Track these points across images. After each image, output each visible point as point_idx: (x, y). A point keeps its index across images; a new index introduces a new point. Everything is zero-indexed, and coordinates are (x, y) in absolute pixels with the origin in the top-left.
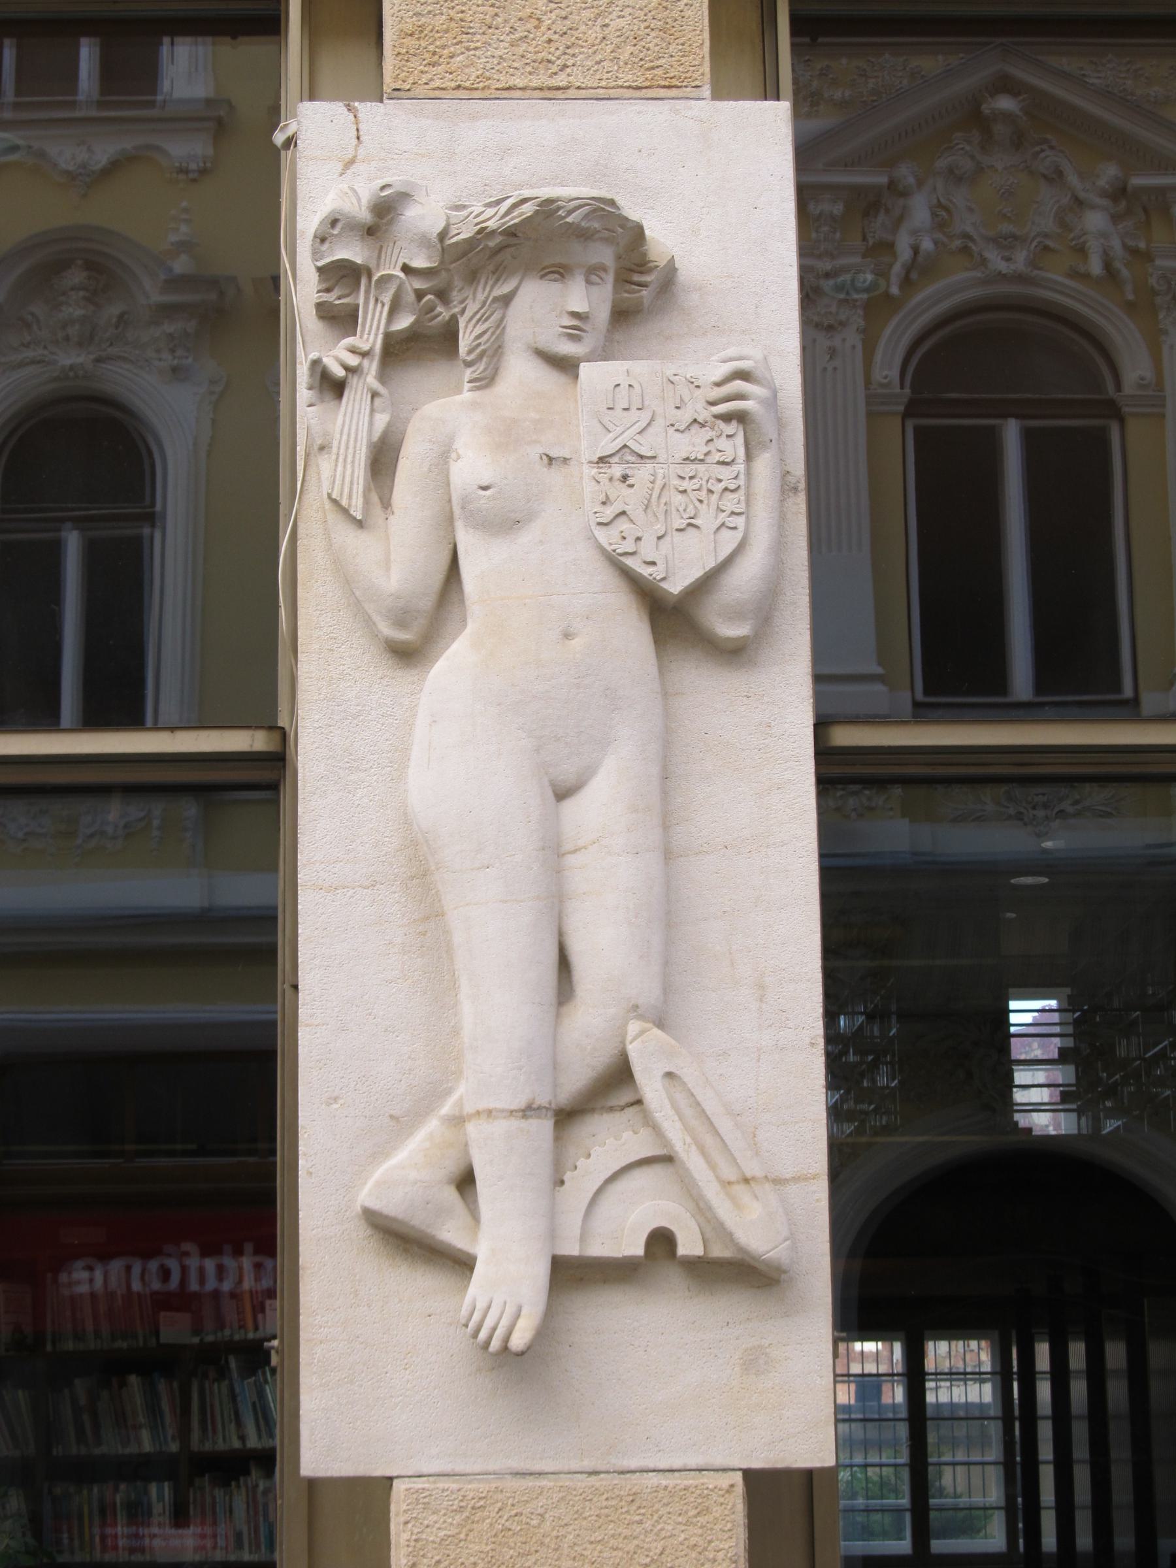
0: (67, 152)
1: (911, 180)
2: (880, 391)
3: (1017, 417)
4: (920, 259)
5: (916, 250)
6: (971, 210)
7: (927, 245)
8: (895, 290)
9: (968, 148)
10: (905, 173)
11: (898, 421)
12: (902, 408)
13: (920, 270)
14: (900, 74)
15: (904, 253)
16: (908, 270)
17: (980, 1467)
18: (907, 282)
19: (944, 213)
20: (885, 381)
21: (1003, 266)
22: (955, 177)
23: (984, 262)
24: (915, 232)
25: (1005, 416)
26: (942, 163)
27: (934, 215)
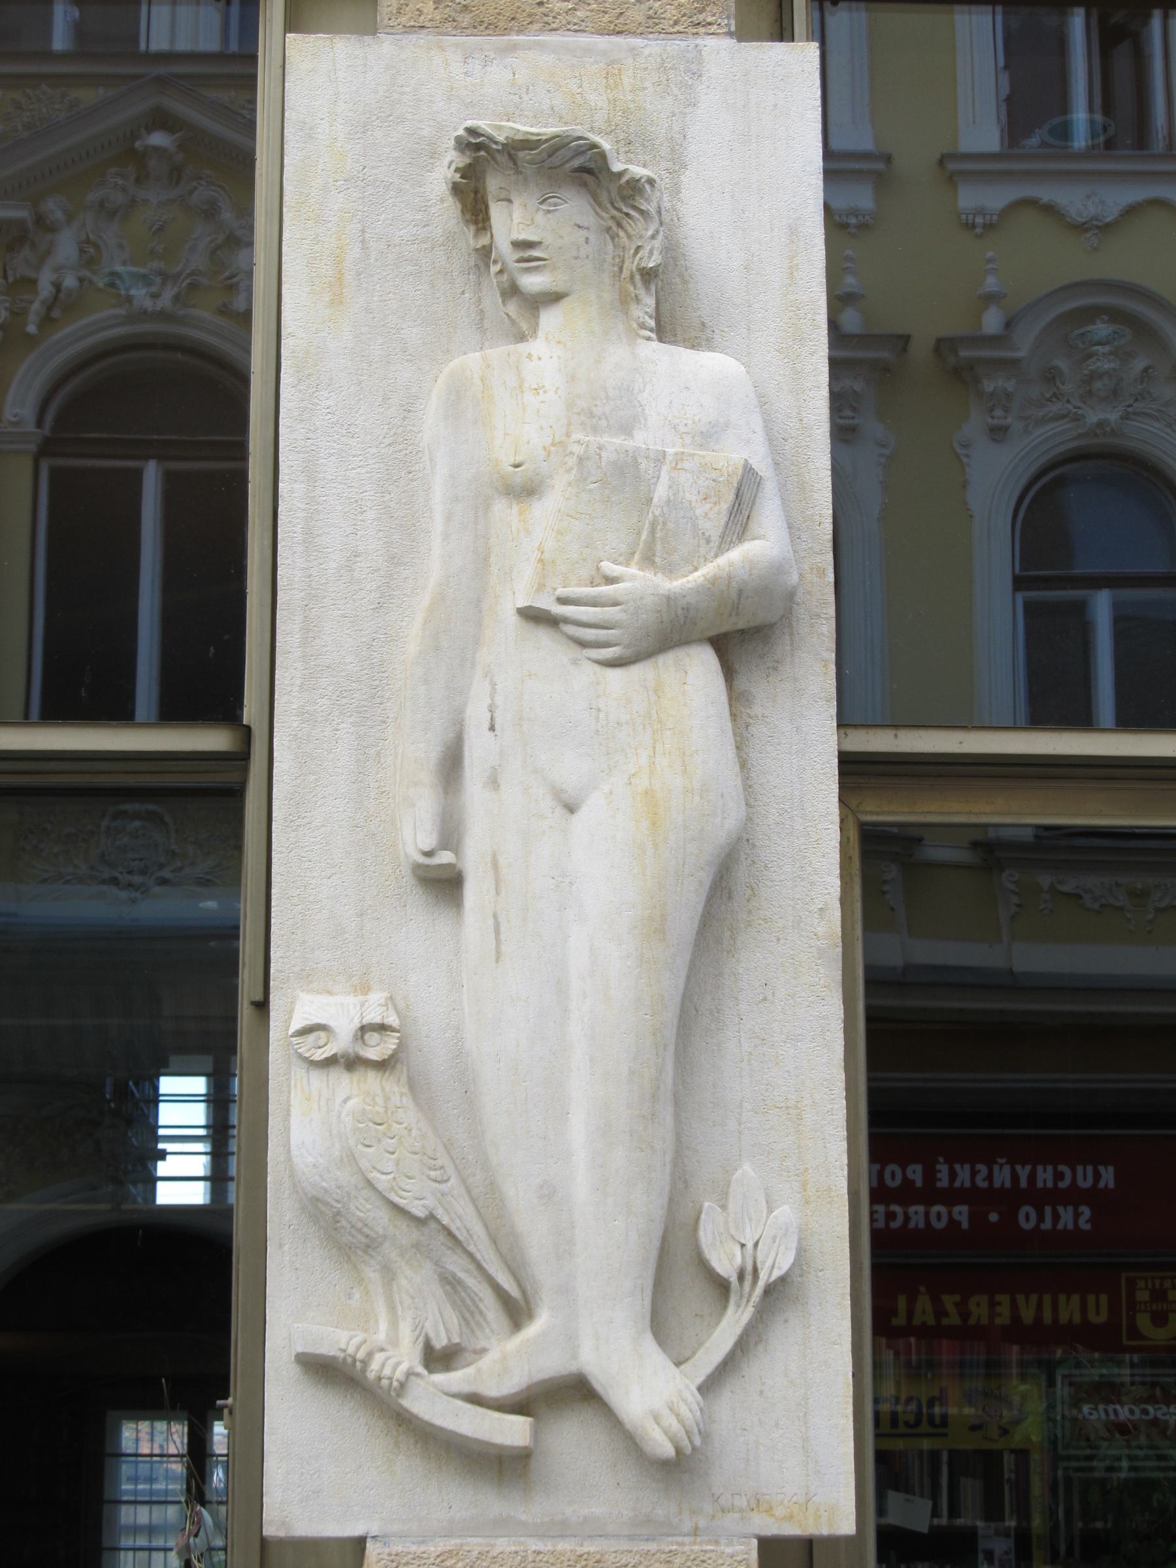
0: (1073, 199)
1: (59, 215)
2: (10, 429)
3: (160, 458)
4: (62, 296)
5: (58, 287)
6: (121, 246)
7: (70, 282)
8: (31, 329)
9: (120, 182)
10: (53, 207)
11: (27, 464)
12: (33, 447)
13: (61, 305)
14: (58, 106)
15: (45, 289)
16: (50, 306)
17: (147, 1553)
18: (48, 321)
19: (92, 250)
20: (14, 419)
21: (148, 304)
22: (105, 210)
23: (129, 299)
24: (58, 269)
25: (147, 458)
26: (93, 196)
27: (82, 251)
